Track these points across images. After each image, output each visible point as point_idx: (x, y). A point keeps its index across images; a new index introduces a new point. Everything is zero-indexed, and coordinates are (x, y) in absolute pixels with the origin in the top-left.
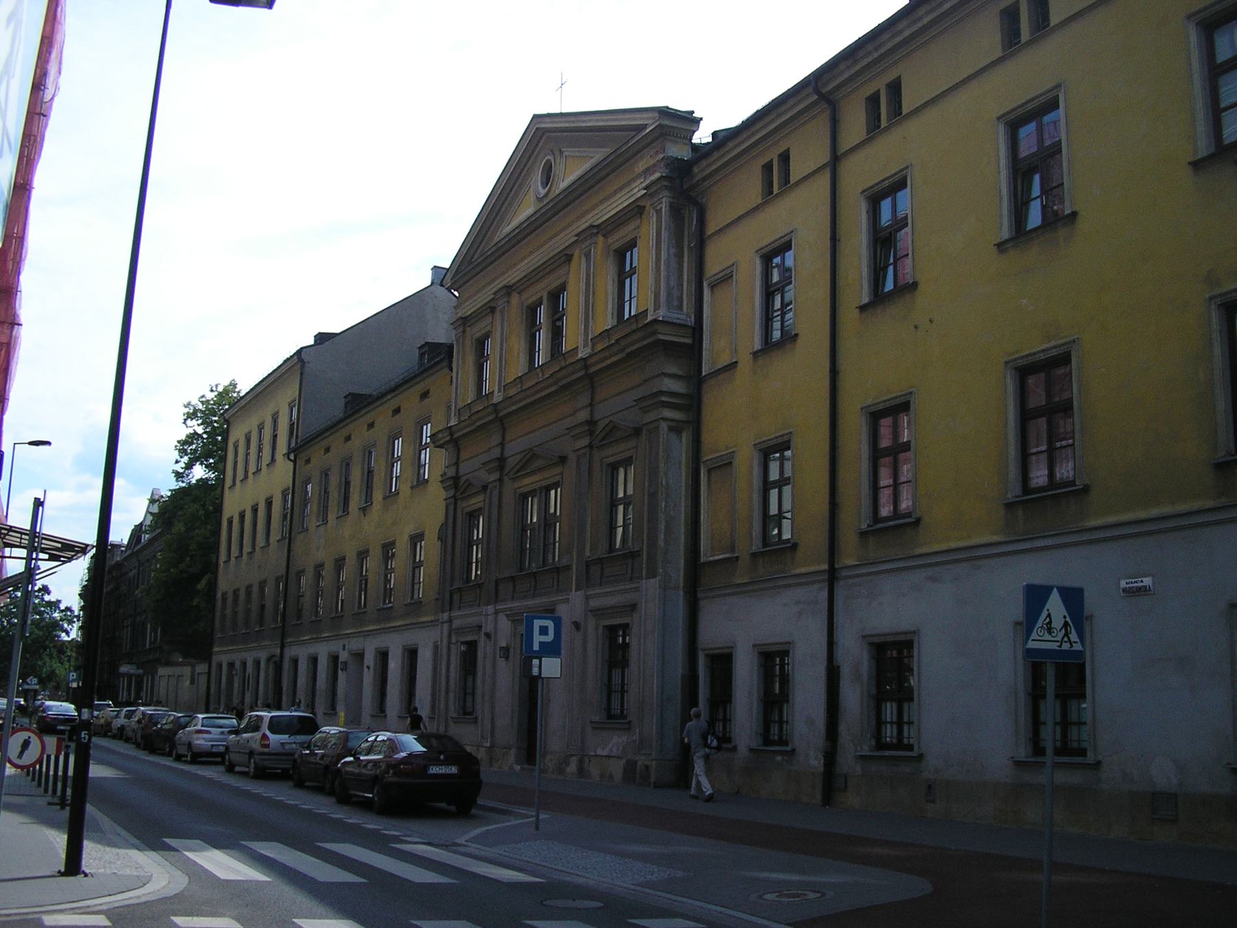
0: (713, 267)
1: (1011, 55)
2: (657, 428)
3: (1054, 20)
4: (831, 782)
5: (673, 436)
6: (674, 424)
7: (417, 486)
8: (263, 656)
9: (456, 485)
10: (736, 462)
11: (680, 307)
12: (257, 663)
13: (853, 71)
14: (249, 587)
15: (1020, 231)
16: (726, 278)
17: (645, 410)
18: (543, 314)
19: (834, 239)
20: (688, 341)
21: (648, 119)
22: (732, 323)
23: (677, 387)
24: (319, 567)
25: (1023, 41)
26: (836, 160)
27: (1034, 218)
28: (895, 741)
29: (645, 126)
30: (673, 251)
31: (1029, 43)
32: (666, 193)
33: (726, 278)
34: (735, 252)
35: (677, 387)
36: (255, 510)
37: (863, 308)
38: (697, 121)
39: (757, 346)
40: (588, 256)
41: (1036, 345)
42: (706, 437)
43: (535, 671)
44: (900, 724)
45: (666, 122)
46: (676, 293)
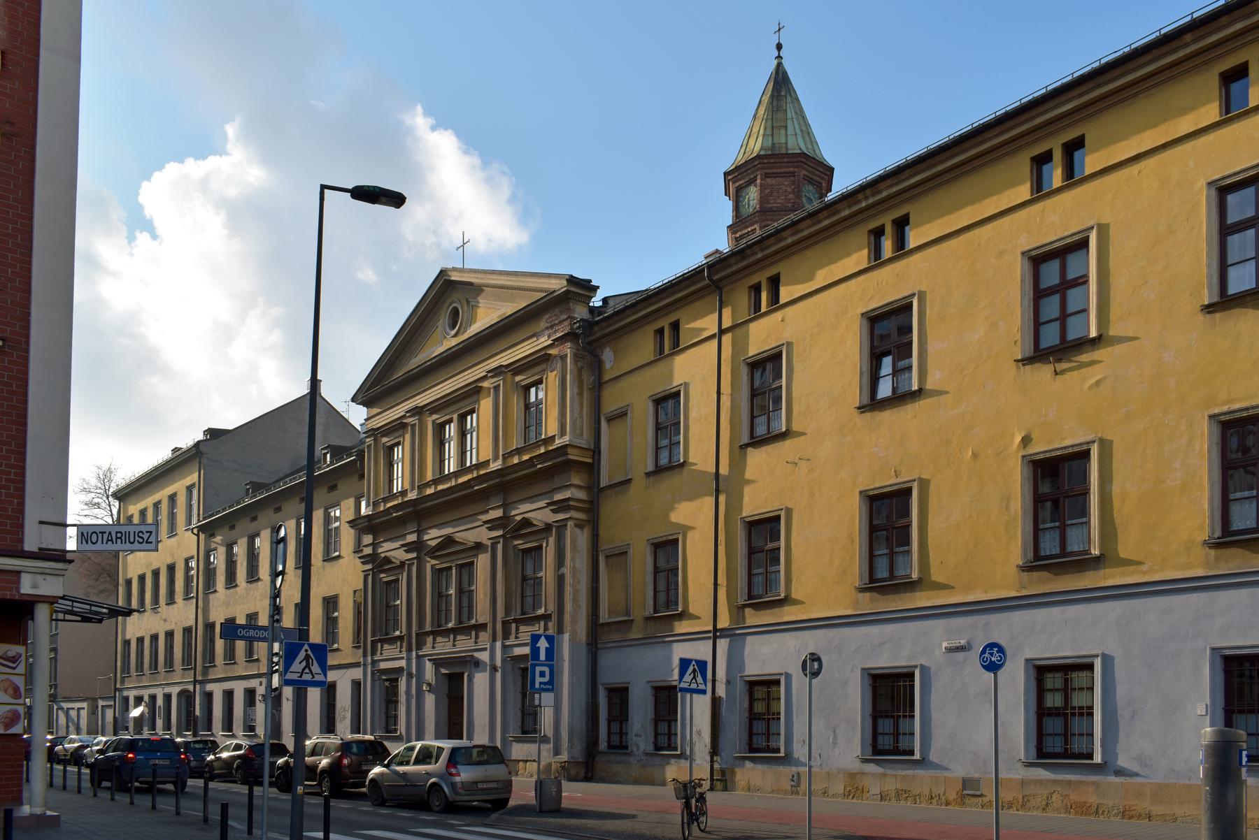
0: (609, 406)
3: (782, 301)
5: (577, 530)
8: (175, 691)
9: (377, 564)
10: (631, 552)
11: (581, 434)
12: (168, 697)
13: (739, 266)
14: (170, 635)
15: (873, 404)
16: (621, 415)
18: (452, 430)
20: (590, 461)
22: (631, 446)
23: (581, 495)
24: (140, 640)
27: (885, 390)
30: (576, 391)
31: (891, 260)
33: (621, 415)
34: (634, 397)
35: (581, 495)
36: (156, 573)
37: (648, 474)
38: (596, 288)
39: (651, 468)
41: (886, 481)
42: (602, 533)
43: (537, 702)
44: (896, 734)
45: (573, 289)
46: (578, 423)
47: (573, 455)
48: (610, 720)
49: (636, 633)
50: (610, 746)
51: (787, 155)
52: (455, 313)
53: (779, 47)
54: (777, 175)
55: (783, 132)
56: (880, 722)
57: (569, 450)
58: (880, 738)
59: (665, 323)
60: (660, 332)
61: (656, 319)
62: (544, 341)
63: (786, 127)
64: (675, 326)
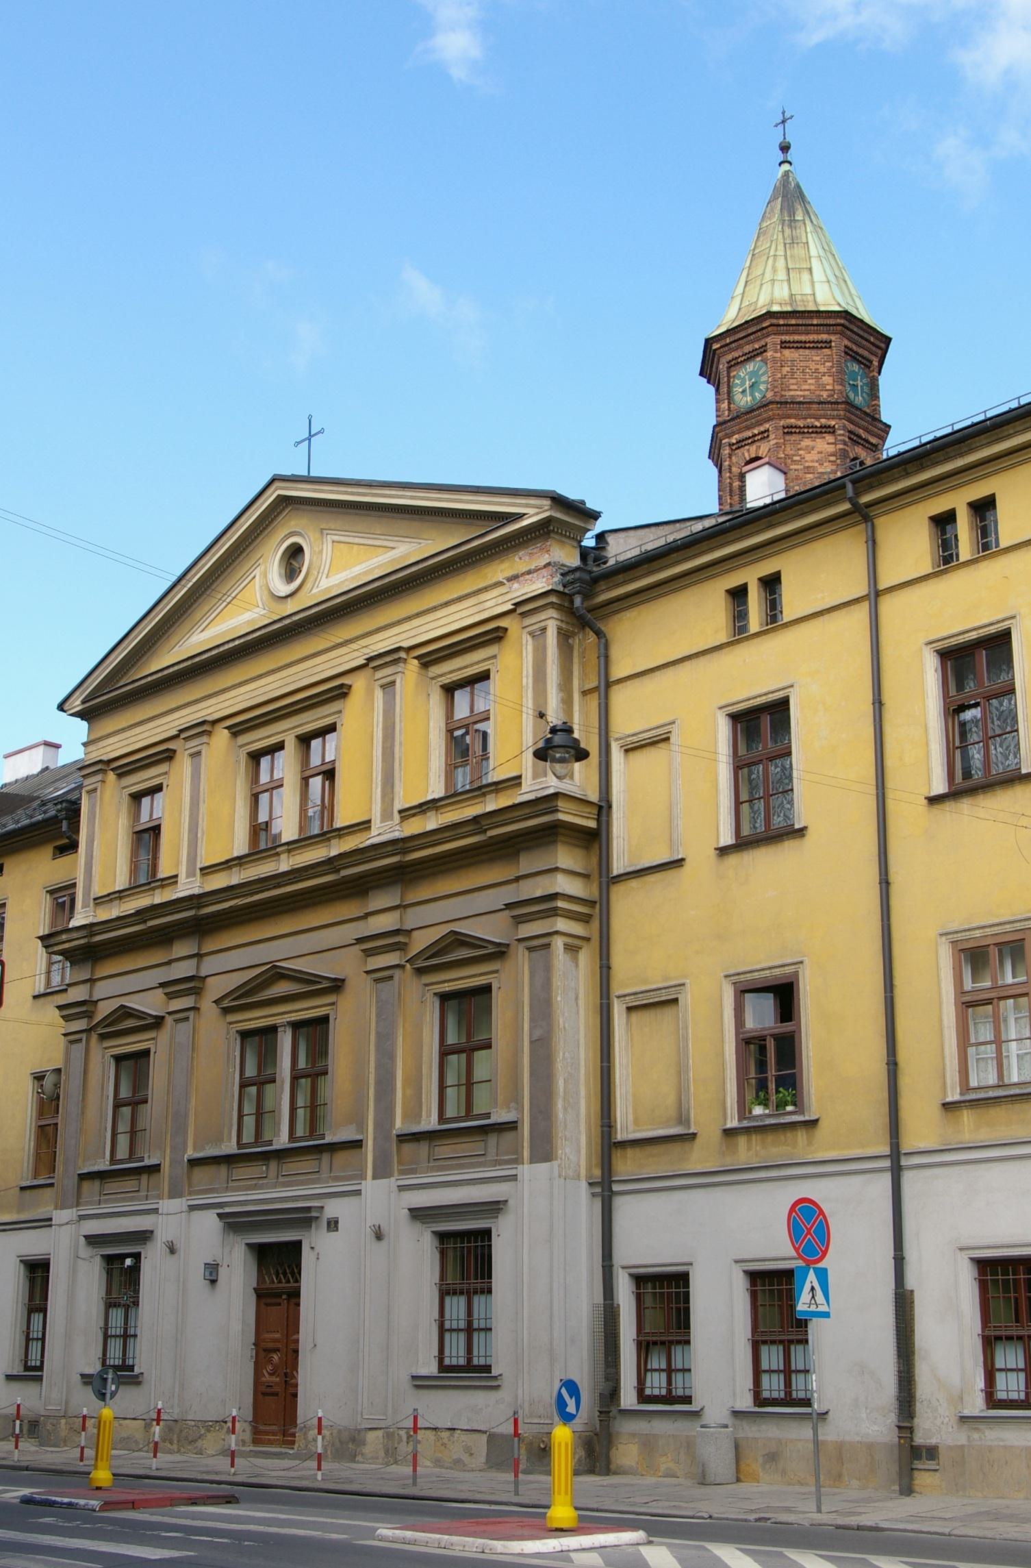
1: (738, 642)
2: (548, 946)
4: (912, 1455)
6: (569, 940)
7: (954, 794)
10: (688, 999)
17: (519, 920)
19: (878, 703)
20: (592, 824)
21: (527, 506)
25: (962, 559)
26: (875, 595)
28: (782, 1395)
29: (520, 516)
32: (551, 613)
38: (594, 516)
40: (389, 686)
44: (787, 1372)
47: (567, 815)
48: (644, 1347)
49: (700, 1157)
50: (643, 1398)
51: (818, 313)
52: (295, 552)
53: (785, 148)
54: (801, 345)
55: (806, 276)
56: (764, 1350)
57: (561, 804)
58: (1000, 1378)
59: (750, 576)
60: (738, 595)
61: (728, 571)
62: (495, 603)
63: (810, 270)
64: (771, 583)
